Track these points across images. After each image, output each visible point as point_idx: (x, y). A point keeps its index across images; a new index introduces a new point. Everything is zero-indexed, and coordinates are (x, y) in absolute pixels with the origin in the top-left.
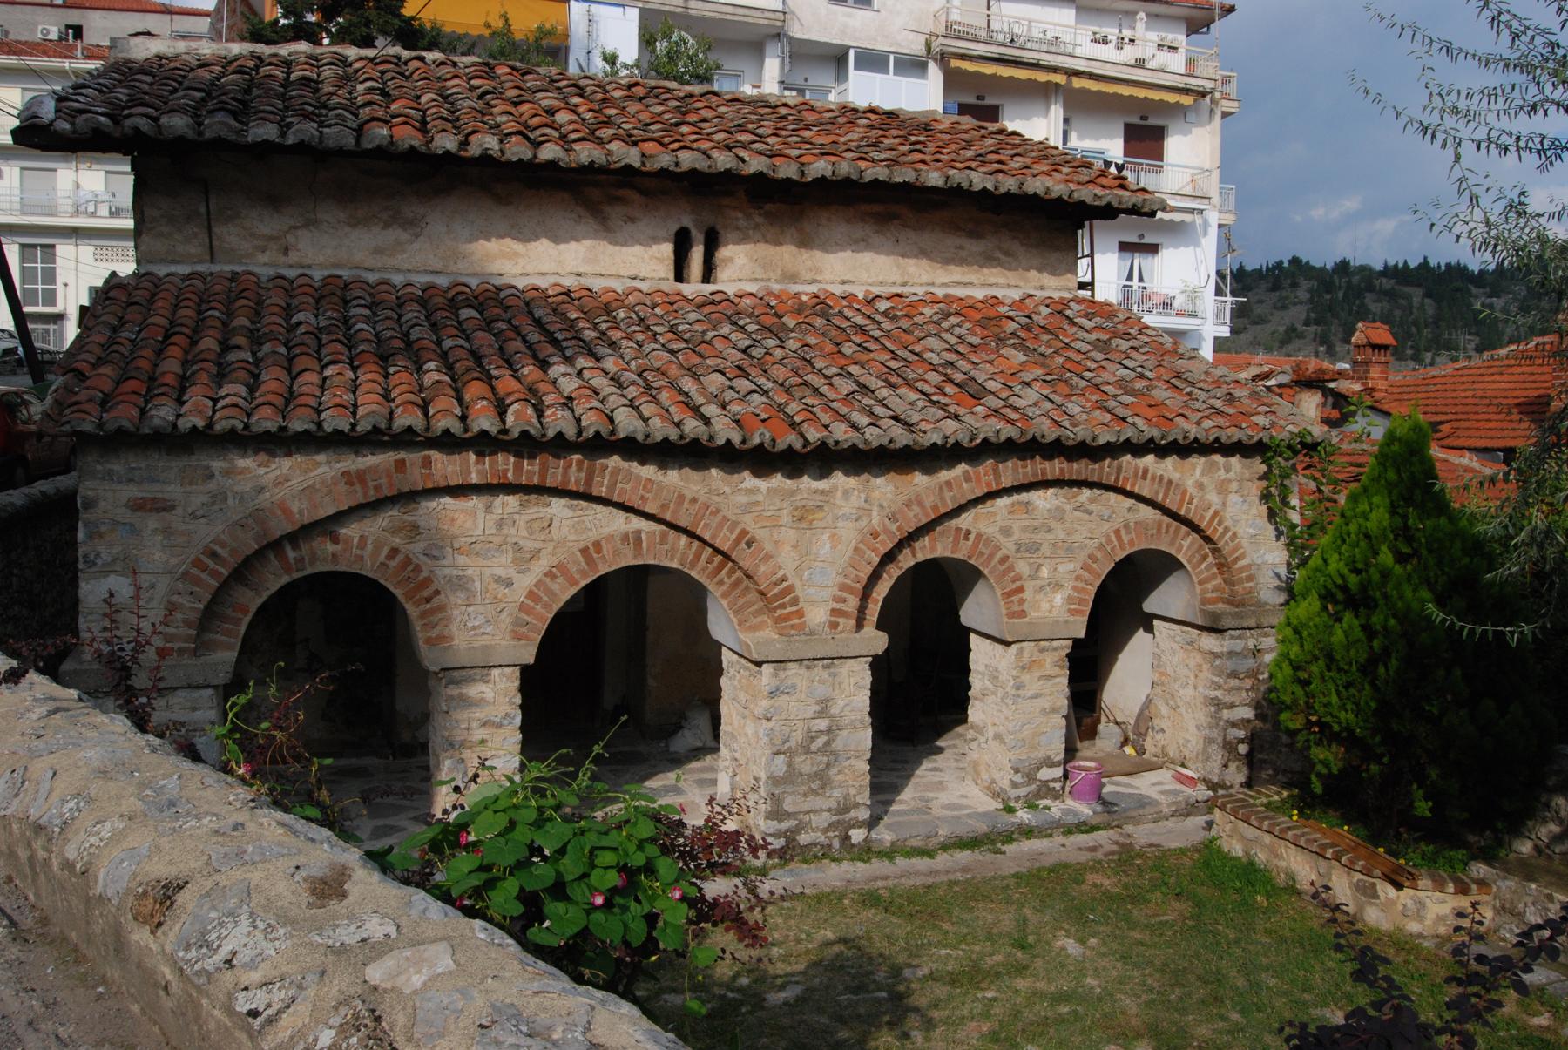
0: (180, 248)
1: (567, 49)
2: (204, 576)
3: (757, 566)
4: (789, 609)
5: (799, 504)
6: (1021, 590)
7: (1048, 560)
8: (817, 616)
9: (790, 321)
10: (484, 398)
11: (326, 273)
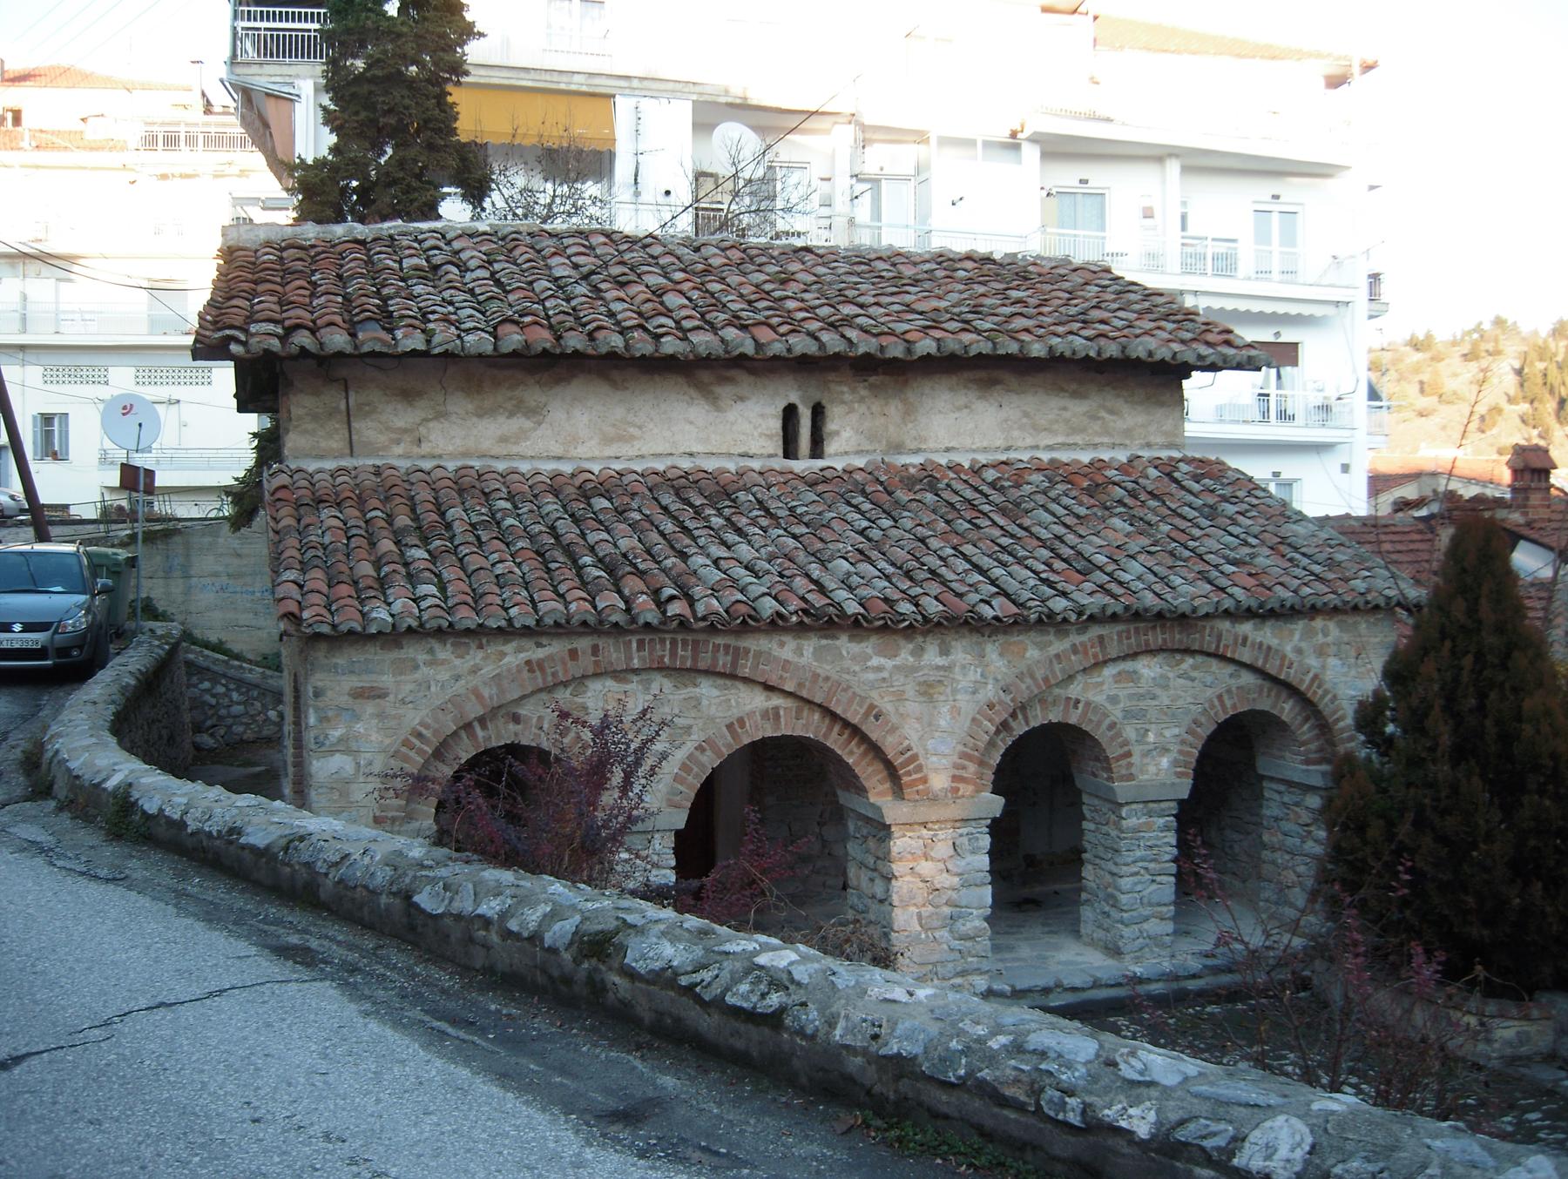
0: (323, 444)
1: (612, 155)
2: (412, 754)
3: (885, 737)
4: (915, 776)
5: (922, 679)
6: (1129, 754)
7: (1153, 726)
9: (902, 495)
10: (643, 593)
11: (459, 464)
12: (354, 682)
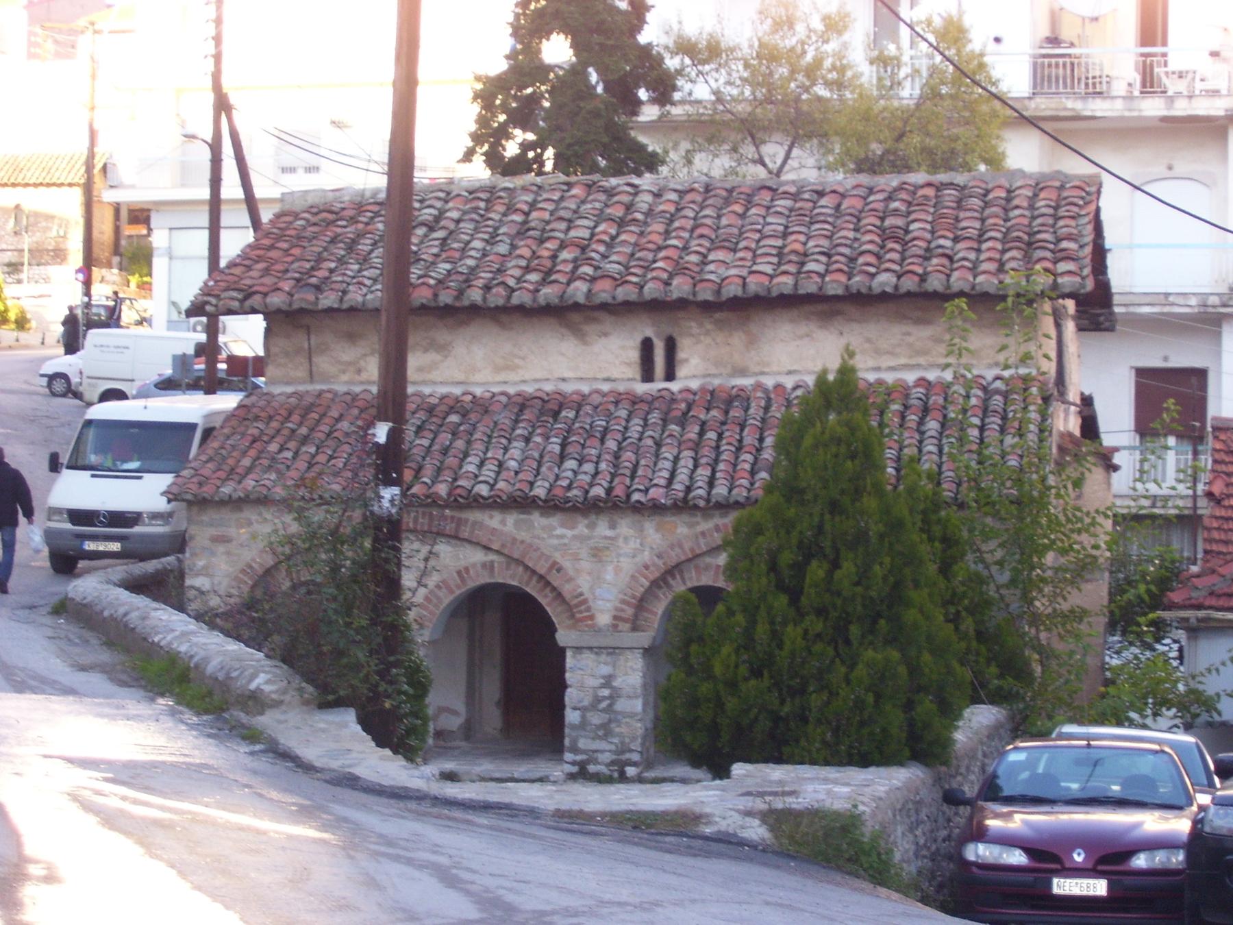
8: (604, 619)
12: (213, 531)
